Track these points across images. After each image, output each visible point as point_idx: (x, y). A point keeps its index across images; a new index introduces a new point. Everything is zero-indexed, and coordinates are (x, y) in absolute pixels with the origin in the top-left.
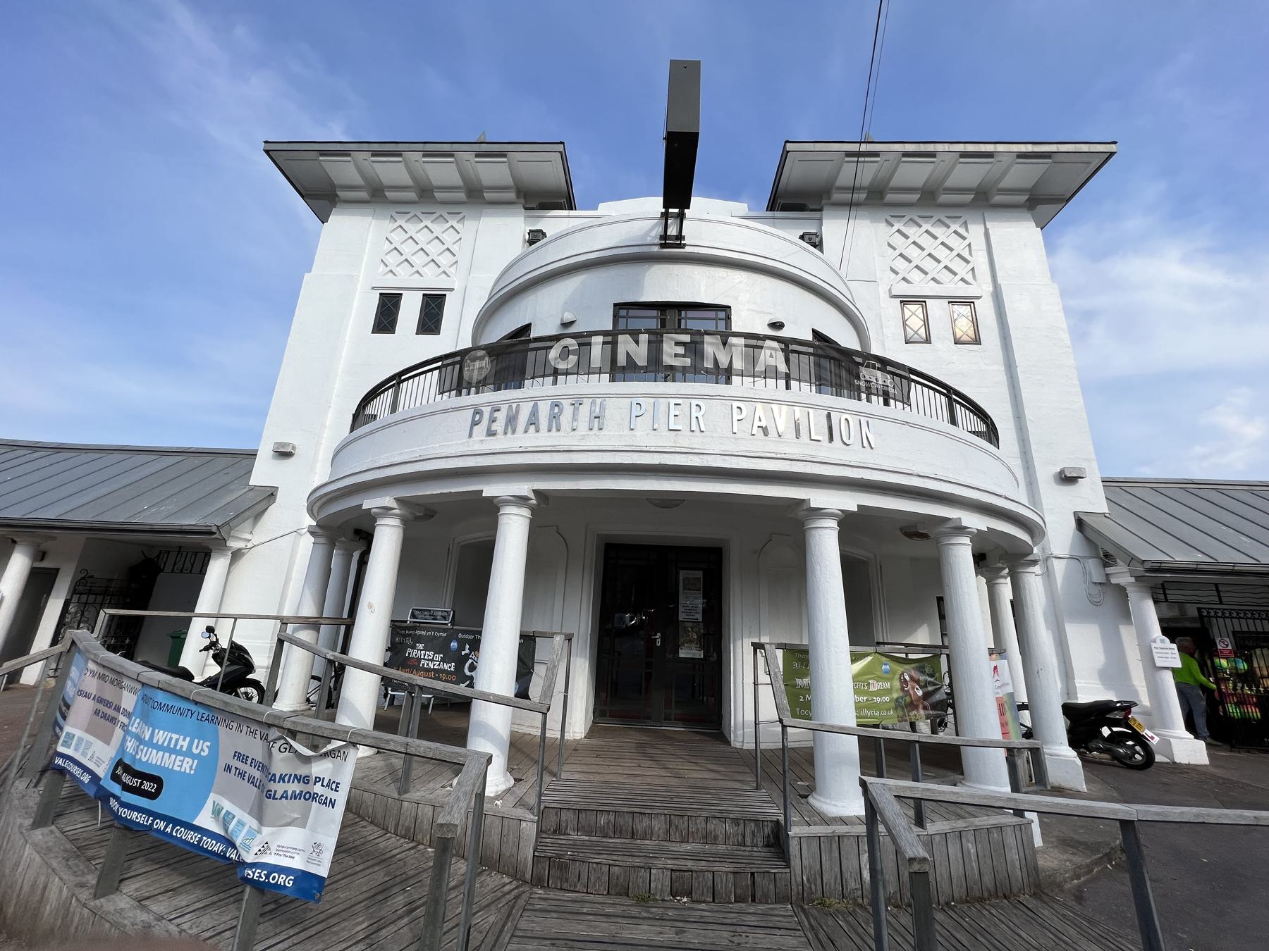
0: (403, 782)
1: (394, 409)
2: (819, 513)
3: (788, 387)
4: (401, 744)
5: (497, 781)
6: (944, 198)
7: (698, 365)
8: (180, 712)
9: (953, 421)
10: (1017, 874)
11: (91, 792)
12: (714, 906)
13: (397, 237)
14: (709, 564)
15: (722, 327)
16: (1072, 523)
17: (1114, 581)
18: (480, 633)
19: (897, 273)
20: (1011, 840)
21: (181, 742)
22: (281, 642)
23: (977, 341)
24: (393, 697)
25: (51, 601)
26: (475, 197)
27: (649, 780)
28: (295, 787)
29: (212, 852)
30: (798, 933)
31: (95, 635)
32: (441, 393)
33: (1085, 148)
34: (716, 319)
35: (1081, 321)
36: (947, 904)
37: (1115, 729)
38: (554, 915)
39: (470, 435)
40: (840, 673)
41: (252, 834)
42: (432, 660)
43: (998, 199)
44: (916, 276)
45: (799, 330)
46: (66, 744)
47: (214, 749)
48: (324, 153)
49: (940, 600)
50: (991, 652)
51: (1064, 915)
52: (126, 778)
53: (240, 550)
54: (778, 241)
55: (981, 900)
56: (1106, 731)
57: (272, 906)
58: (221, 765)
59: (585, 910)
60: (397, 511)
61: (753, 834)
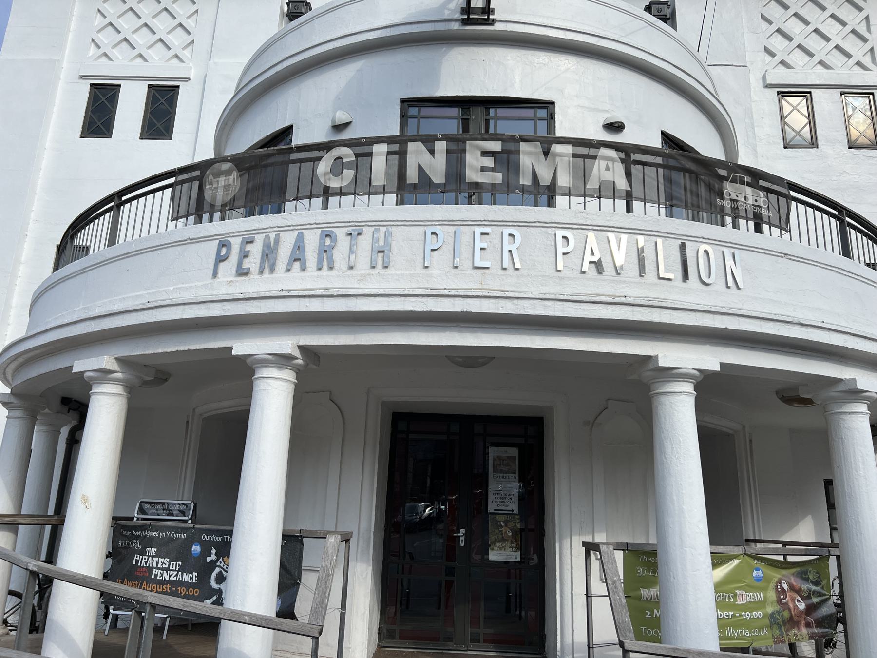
2: (670, 374)
3: (629, 210)
9: (846, 251)
14: (527, 438)
15: (542, 131)
18: (230, 533)
19: (773, 55)
24: (116, 617)
32: (175, 219)
34: (535, 119)
39: (215, 275)
42: (167, 570)
44: (798, 58)
49: (829, 483)
60: (119, 375)
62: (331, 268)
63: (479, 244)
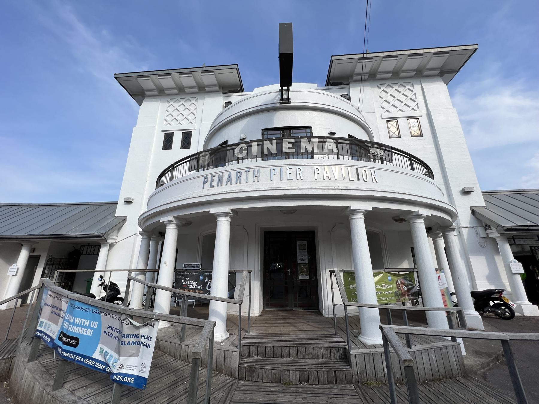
0: (182, 336)
1: (171, 179)
2: (355, 212)
3: (338, 158)
4: (177, 319)
5: (220, 334)
6: (402, 75)
7: (299, 152)
8: (85, 310)
9: (412, 169)
10: (455, 367)
11: (50, 346)
12: (318, 386)
13: (171, 109)
14: (309, 238)
15: (308, 135)
16: (470, 212)
17: (490, 236)
18: (212, 272)
19: (384, 108)
20: (451, 352)
21: (86, 323)
22: (129, 280)
23: (421, 135)
24: (178, 302)
25: (38, 269)
26: (202, 90)
27: (288, 332)
28: (133, 340)
29: (100, 369)
30: (357, 397)
31: (53, 281)
32: (191, 171)
33: (464, 48)
34: (306, 133)
35: (468, 125)
36: (424, 382)
37: (496, 302)
38: (249, 392)
39: (203, 188)
40: (369, 281)
41: (116, 360)
42: (192, 285)
43: (426, 73)
44: (392, 109)
45: (342, 134)
46: (41, 326)
47: (100, 325)
48: (139, 77)
49: (412, 249)
50: (437, 270)
51: (478, 386)
52: (64, 339)
53: (113, 243)
54: (331, 98)
55: (439, 380)
56: (491, 303)
57: (127, 392)
58: (103, 332)
59: (262, 390)
60: (175, 222)
61: (335, 354)
62: (240, 183)
63: (289, 172)
